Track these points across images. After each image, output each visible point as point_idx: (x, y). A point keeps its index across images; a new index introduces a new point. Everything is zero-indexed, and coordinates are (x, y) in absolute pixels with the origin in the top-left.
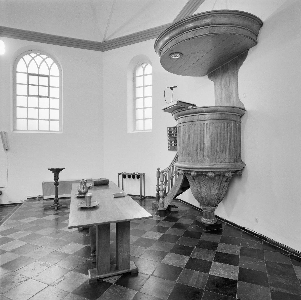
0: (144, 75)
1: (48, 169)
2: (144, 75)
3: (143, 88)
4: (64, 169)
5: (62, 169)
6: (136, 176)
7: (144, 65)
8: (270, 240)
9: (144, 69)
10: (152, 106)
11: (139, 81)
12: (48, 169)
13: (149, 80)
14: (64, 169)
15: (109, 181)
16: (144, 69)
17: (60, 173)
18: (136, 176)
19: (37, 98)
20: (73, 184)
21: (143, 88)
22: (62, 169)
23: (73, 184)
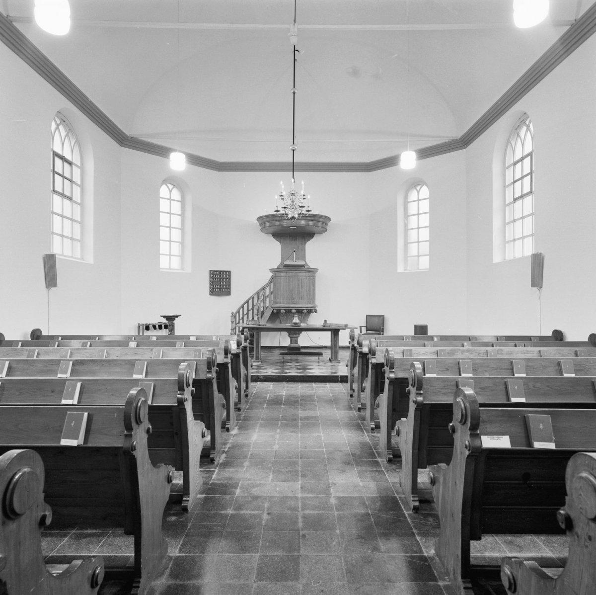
0: (418, 200)
1: (161, 316)
2: (418, 200)
3: (417, 216)
4: (180, 316)
5: (177, 316)
6: (163, 326)
7: (418, 188)
8: (296, 426)
9: (418, 192)
10: (428, 253)
11: (413, 208)
12: (161, 316)
13: (425, 206)
14: (180, 316)
15: (319, 271)
16: (418, 192)
17: (52, 288)
18: (163, 326)
19: (299, 158)
20: (131, 540)
21: (420, 212)
22: (177, 316)
23: (131, 540)
